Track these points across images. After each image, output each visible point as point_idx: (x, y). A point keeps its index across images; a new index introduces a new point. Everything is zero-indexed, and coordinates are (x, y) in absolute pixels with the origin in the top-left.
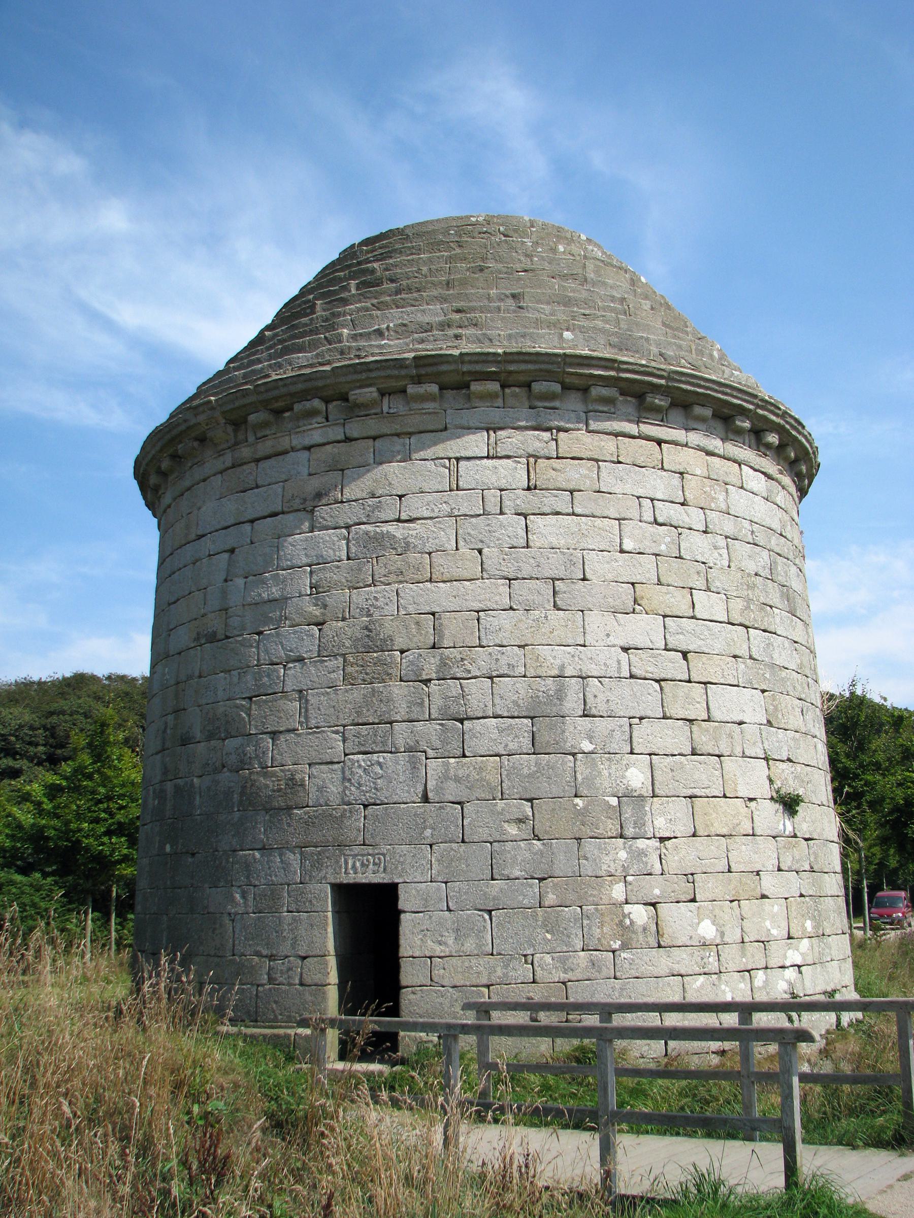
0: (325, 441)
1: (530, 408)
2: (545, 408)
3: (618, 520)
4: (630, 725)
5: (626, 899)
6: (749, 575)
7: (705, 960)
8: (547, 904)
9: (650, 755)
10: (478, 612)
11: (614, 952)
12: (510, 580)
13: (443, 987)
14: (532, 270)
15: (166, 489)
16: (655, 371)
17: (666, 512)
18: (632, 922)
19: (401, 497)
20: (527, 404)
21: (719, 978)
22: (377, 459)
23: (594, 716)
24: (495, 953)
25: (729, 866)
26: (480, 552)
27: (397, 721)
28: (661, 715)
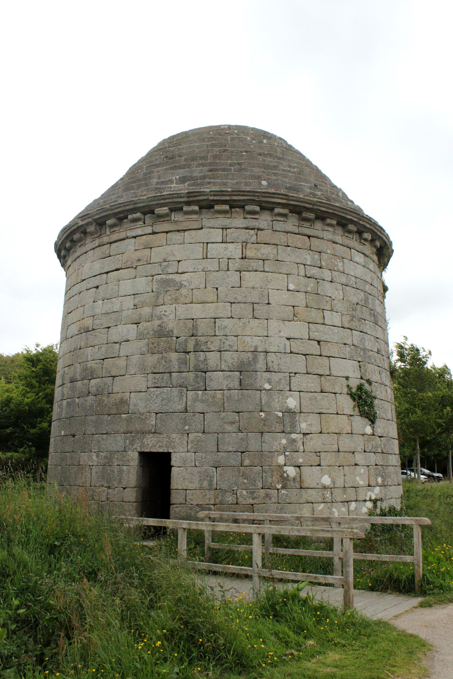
0: (143, 233)
1: (244, 218)
2: (252, 218)
3: (287, 274)
4: (290, 377)
5: (285, 464)
6: (353, 304)
7: (325, 496)
8: (245, 464)
9: (299, 392)
10: (215, 319)
11: (278, 490)
12: (231, 303)
13: (192, 504)
14: (249, 152)
15: (69, 257)
16: (307, 201)
17: (314, 271)
18: (288, 475)
19: (179, 261)
20: (242, 216)
21: (332, 506)
22: (168, 242)
23: (271, 372)
24: (218, 488)
25: (339, 449)
26: (217, 289)
27: (174, 372)
28: (306, 372)
